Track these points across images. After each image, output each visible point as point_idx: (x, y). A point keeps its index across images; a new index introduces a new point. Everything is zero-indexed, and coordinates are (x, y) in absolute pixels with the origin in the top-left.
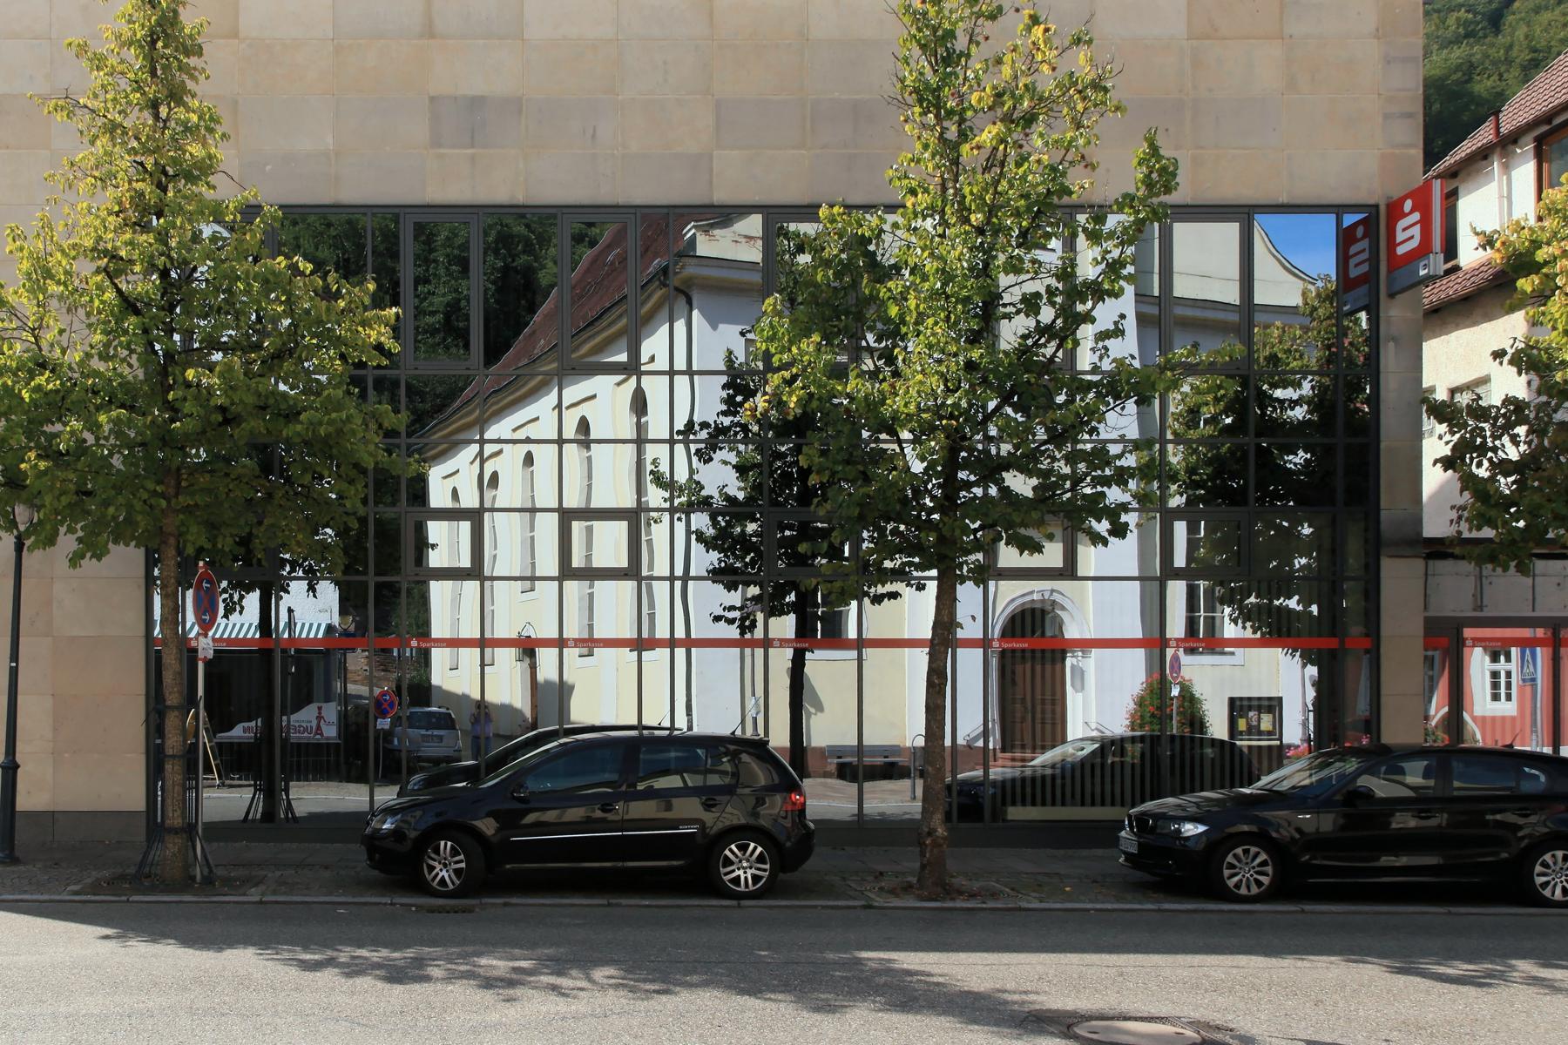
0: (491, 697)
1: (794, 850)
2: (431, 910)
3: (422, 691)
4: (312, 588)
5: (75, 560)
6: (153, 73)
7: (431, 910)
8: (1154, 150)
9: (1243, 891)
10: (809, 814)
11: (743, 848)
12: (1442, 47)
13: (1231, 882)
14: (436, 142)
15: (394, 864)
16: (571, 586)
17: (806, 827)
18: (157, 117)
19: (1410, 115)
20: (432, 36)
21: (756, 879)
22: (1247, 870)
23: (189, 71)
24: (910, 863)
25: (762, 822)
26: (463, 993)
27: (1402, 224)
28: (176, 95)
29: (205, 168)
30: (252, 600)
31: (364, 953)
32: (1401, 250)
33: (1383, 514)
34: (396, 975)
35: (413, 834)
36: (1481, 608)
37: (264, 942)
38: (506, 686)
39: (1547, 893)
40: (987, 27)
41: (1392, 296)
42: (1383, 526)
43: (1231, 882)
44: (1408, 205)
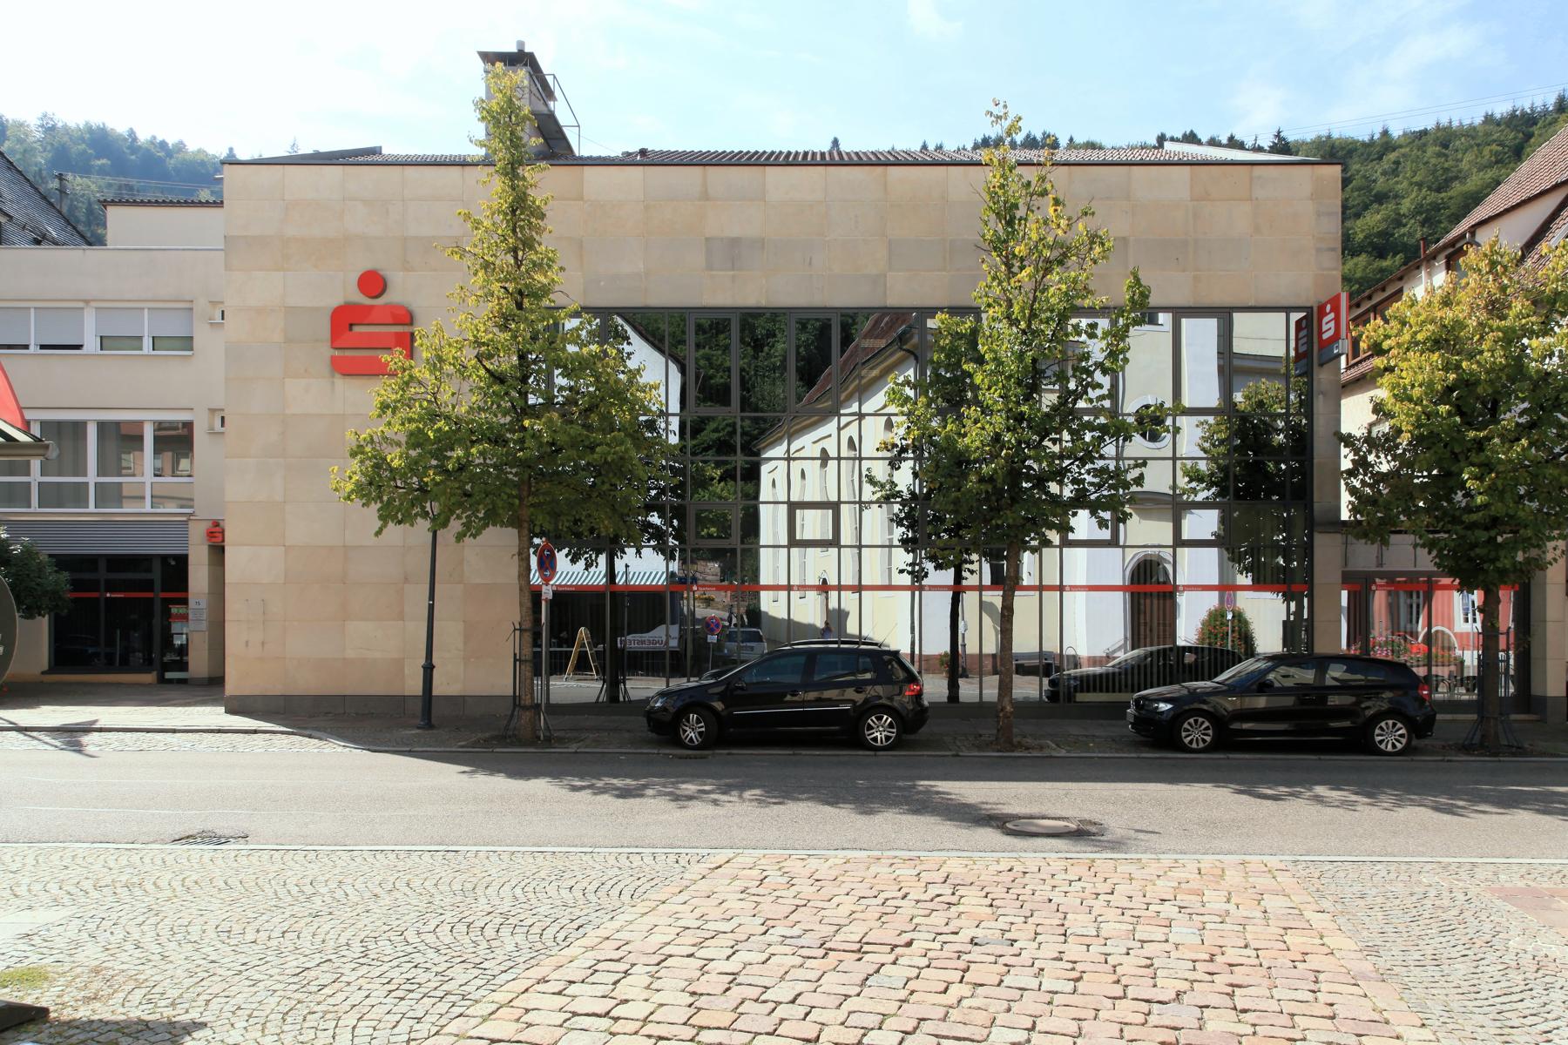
0: (796, 617)
1: (914, 724)
2: (681, 757)
3: (755, 615)
4: (638, 552)
5: (460, 537)
6: (514, 231)
7: (681, 757)
8: (1138, 280)
9: (1194, 746)
10: (925, 696)
11: (880, 719)
12: (1480, 170)
13: (1187, 740)
14: (710, 267)
15: (662, 727)
16: (794, 551)
17: (921, 705)
18: (516, 258)
19: (1333, 249)
20: (708, 199)
21: (888, 738)
22: (1197, 733)
23: (540, 231)
24: (989, 732)
25: (896, 704)
26: (662, 804)
27: (1325, 320)
28: (529, 244)
29: (545, 291)
30: (602, 559)
31: (615, 781)
32: (1325, 336)
33: (1316, 506)
34: (624, 794)
35: (672, 710)
36: (1381, 565)
37: (555, 774)
38: (809, 611)
39: (1383, 746)
40: (1037, 201)
41: (1321, 365)
42: (1316, 513)
43: (1187, 740)
44: (1328, 308)
